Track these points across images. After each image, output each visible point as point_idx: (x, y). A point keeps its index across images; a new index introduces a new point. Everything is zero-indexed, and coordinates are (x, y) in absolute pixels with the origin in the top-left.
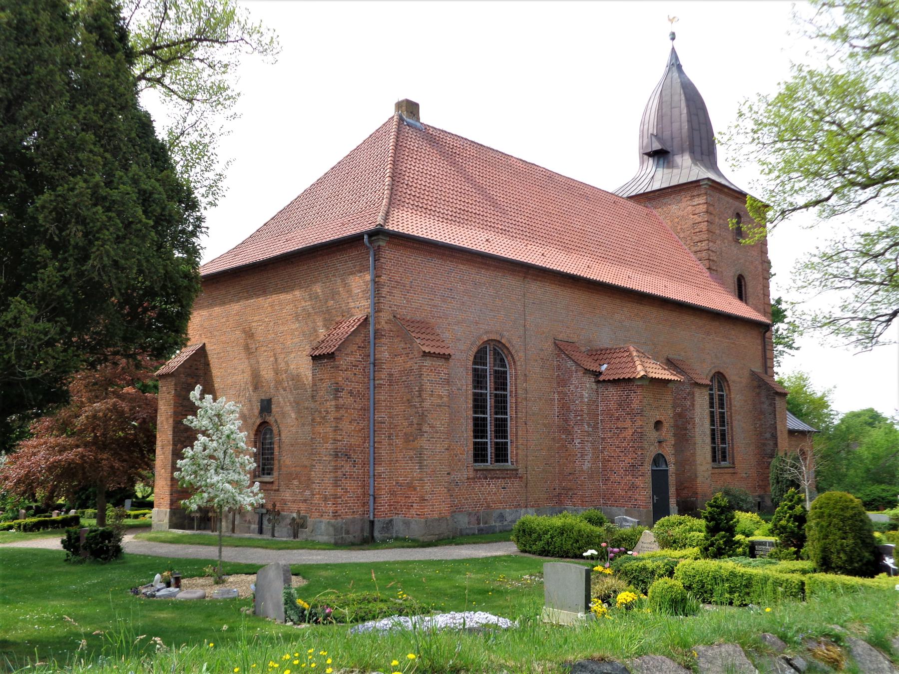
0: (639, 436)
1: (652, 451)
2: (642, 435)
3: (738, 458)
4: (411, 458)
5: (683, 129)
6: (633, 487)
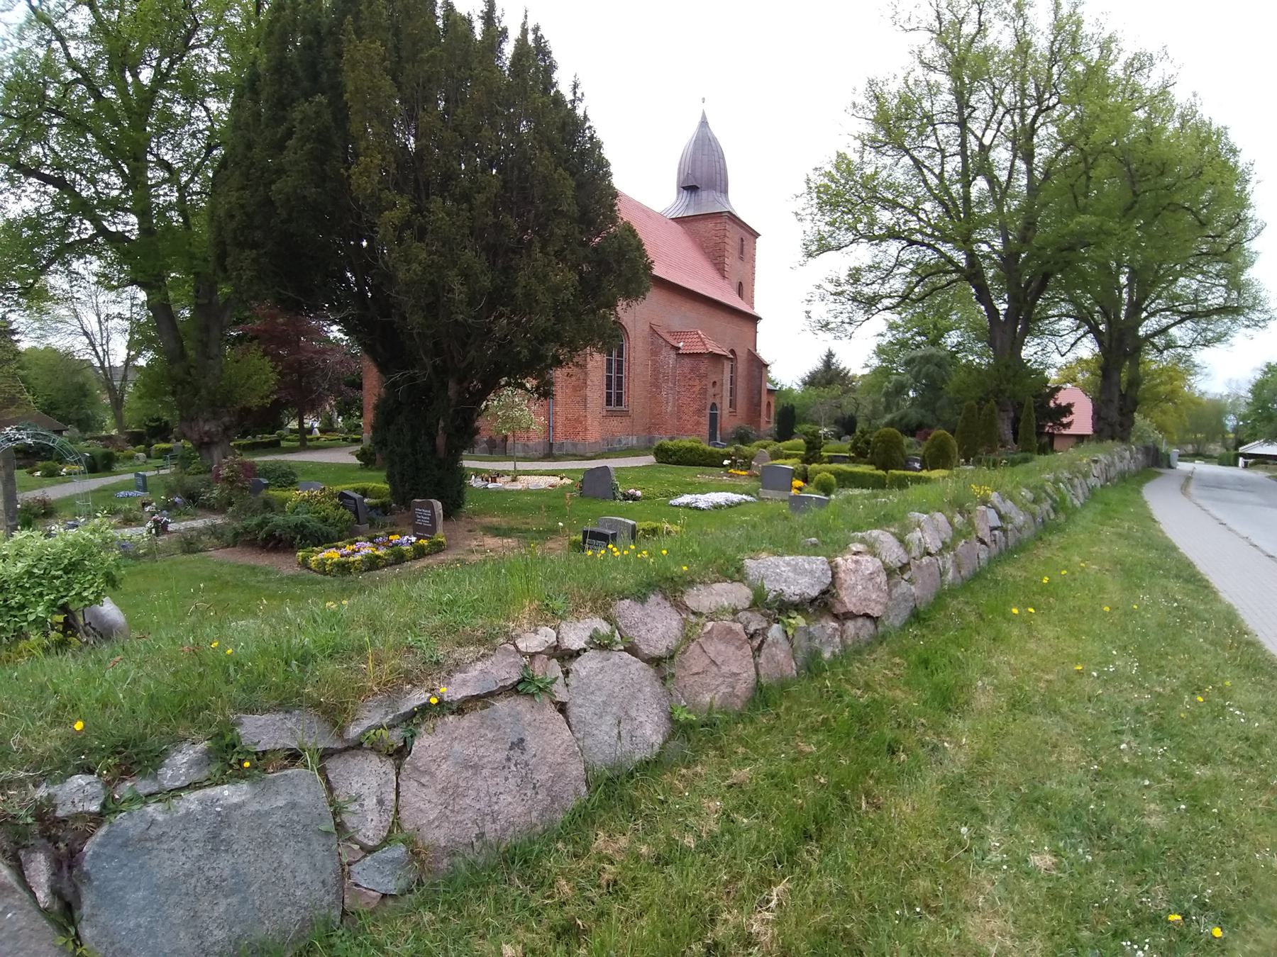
0: (704, 391)
1: (710, 401)
2: (706, 391)
6: (698, 423)
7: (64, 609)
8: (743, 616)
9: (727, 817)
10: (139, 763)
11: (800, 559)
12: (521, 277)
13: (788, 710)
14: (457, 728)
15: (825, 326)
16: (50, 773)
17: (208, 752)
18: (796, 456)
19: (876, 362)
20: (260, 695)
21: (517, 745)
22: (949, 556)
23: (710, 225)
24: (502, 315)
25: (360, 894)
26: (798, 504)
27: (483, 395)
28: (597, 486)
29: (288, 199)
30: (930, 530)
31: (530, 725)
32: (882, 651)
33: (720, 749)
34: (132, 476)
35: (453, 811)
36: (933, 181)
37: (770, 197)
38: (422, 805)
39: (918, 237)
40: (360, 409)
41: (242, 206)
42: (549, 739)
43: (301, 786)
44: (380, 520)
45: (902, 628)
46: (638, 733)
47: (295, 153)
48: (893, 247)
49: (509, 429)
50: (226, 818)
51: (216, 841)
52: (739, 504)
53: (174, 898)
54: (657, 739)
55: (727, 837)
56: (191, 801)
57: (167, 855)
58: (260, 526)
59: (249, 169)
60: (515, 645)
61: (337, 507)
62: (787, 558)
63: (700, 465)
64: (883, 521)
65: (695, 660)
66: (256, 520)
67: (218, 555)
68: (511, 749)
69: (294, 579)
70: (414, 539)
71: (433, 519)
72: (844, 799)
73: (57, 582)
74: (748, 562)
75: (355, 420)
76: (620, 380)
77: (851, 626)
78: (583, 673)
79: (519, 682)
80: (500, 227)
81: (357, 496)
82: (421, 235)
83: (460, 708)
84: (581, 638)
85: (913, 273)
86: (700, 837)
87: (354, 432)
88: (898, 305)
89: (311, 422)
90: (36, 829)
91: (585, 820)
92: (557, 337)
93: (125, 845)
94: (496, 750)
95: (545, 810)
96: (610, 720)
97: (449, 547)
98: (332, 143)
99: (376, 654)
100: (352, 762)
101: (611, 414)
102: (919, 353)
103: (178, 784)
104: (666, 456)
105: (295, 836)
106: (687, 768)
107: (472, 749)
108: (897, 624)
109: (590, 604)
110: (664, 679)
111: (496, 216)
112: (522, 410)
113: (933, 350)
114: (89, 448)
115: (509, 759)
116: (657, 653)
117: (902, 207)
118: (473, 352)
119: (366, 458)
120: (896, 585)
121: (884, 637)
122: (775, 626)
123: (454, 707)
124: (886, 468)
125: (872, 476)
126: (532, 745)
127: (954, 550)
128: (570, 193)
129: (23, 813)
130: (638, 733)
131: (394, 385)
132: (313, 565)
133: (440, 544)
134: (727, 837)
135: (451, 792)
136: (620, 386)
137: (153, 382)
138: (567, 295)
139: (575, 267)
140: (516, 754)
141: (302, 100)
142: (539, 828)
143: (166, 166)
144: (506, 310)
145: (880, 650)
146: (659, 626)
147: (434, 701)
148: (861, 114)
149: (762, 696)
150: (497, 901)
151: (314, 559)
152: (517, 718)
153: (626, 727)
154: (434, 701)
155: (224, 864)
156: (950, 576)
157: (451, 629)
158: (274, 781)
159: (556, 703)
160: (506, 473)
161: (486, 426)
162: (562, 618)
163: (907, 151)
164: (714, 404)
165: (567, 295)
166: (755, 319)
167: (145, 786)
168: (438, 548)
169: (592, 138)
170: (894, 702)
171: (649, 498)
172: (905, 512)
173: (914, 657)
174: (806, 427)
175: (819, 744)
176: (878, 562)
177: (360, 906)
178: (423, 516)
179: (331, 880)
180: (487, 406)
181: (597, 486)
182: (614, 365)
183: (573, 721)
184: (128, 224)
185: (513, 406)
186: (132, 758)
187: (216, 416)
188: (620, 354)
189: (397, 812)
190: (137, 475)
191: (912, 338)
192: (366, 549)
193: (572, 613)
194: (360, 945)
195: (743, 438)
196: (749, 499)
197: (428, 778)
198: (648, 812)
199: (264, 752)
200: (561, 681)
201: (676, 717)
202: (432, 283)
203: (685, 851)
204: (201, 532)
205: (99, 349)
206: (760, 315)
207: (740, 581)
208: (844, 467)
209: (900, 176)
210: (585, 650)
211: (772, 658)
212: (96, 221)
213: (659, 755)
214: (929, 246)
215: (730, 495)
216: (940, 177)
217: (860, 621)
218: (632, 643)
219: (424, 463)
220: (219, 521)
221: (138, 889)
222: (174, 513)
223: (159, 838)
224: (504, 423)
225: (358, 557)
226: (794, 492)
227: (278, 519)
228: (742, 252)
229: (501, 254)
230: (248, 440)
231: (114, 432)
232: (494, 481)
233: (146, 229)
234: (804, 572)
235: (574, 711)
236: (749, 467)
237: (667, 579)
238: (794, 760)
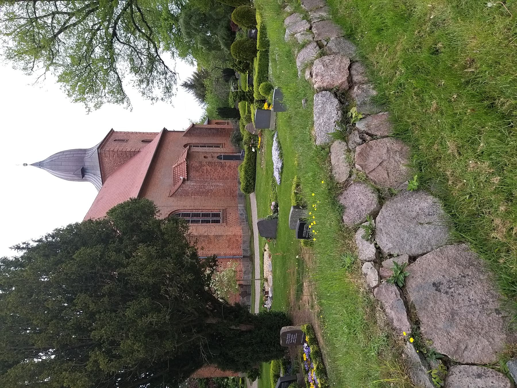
1: (216, 160)
3: (219, 142)
4: (218, 240)
6: (230, 167)
8: (351, 146)
9: (480, 156)
11: (315, 111)
12: (142, 279)
13: (409, 117)
15: (168, 89)
18: (249, 107)
19: (190, 57)
21: (437, 287)
22: (312, 15)
23: (106, 160)
26: (279, 107)
27: (215, 301)
28: (269, 229)
30: (296, 28)
31: (424, 279)
32: (372, 58)
33: (435, 159)
35: (482, 329)
36: (74, 20)
37: (87, 126)
39: (111, 30)
40: (223, 379)
42: (432, 267)
44: (294, 366)
45: (357, 45)
46: (427, 211)
48: (118, 46)
49: (236, 284)
52: (279, 142)
54: (430, 199)
55: (493, 157)
62: (315, 119)
64: (290, 58)
65: (380, 175)
68: (440, 291)
70: (306, 345)
71: (293, 332)
72: (468, 83)
74: (318, 143)
76: (204, 215)
77: (356, 78)
78: (390, 245)
79: (397, 285)
80: (111, 294)
82: (114, 344)
83: (416, 323)
85: (133, 33)
86: (493, 173)
87: (238, 382)
88: (154, 43)
91: (484, 245)
92: (180, 256)
94: (441, 300)
95: (478, 270)
96: (419, 229)
97: (310, 321)
99: (384, 377)
101: (225, 220)
102: (183, 30)
104: (250, 186)
106: (448, 180)
108: (354, 48)
109: (347, 241)
110: (392, 195)
111: (104, 296)
112: (223, 276)
113: (181, 20)
115: (447, 293)
116: (376, 200)
117: (92, 39)
118: (189, 309)
119: (255, 375)
120: (330, 50)
121: (363, 57)
122: (357, 126)
123: (415, 327)
124: (255, 51)
125: (260, 60)
126: (437, 278)
127: (307, 12)
130: (427, 211)
131: (209, 358)
133: (308, 328)
134: (493, 157)
135: (470, 329)
136: (207, 215)
138: (153, 250)
139: (135, 245)
140: (443, 288)
142: (491, 274)
145: (372, 59)
146: (359, 197)
147: (412, 340)
148: (31, 65)
149: (401, 134)
152: (420, 287)
153: (423, 219)
154: (412, 340)
156: (324, 14)
160: (262, 285)
162: (356, 258)
163: (55, 36)
164: (218, 157)
165: (153, 250)
166: (165, 131)
168: (311, 329)
169: (53, 236)
170: (405, 50)
171: (276, 197)
172: (285, 44)
173: (376, 38)
174: (231, 100)
175: (431, 98)
176: (316, 62)
178: (291, 339)
180: (222, 299)
181: (269, 229)
182: (195, 219)
183: (420, 252)
185: (221, 281)
188: (188, 215)
189: (485, 365)
191: (173, 34)
192: (313, 375)
193: (353, 252)
195: (238, 139)
196: (275, 136)
198: (477, 205)
200: (396, 260)
201: (416, 188)
202: (146, 336)
203: (502, 182)
206: (162, 129)
207: (330, 147)
208: (255, 77)
209: (72, 41)
210: (376, 244)
211: (378, 128)
213: (440, 198)
214: (116, 23)
215: (273, 148)
216: (71, 15)
217: (353, 72)
218: (370, 215)
225: (318, 381)
226: (271, 108)
228: (123, 140)
232: (267, 293)
234: (323, 108)
235: (415, 251)
236: (256, 136)
238: (442, 114)
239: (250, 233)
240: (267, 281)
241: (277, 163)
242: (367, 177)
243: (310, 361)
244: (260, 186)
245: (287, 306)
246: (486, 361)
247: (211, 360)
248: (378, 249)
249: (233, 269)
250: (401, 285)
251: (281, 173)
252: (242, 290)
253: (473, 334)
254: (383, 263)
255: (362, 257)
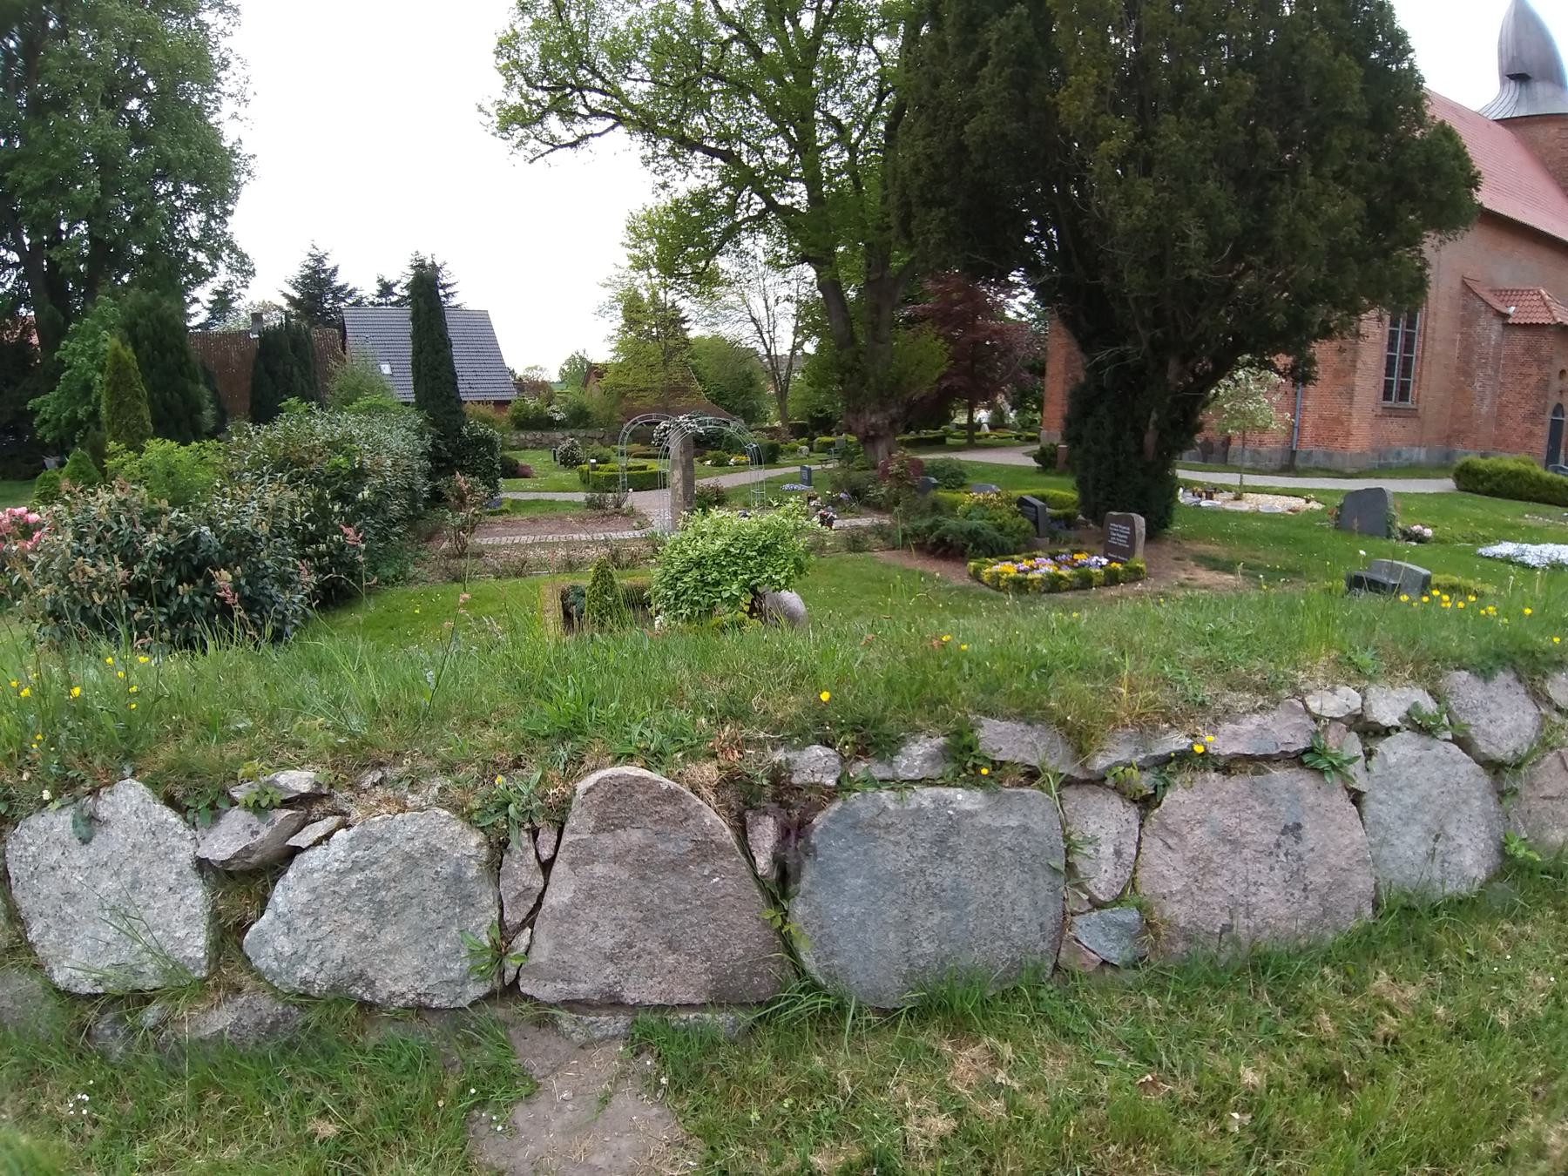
0: (1544, 384)
4: (1340, 394)
5: (355, 290)
6: (1531, 434)
7: (753, 590)
10: (877, 745)
14: (1220, 789)
16: (790, 738)
17: (944, 748)
20: (998, 700)
24: (1249, 267)
25: (1078, 951)
27: (1212, 379)
28: (1365, 515)
29: (985, 142)
31: (1312, 809)
34: (798, 469)
38: (1165, 872)
41: (930, 157)
42: (1335, 835)
43: (1031, 812)
44: (1064, 534)
46: (1454, 858)
47: (991, 83)
50: (957, 823)
51: (942, 846)
53: (891, 895)
56: (924, 797)
57: (892, 848)
58: (931, 529)
59: (936, 109)
60: (1303, 701)
61: (1015, 514)
63: (1529, 499)
66: (926, 522)
67: (884, 556)
68: (1283, 833)
69: (964, 591)
70: (1104, 561)
71: (1132, 540)
73: (751, 563)
75: (1030, 416)
76: (1407, 363)
78: (1392, 759)
79: (1306, 751)
80: (1253, 147)
81: (1038, 503)
82: (1146, 171)
83: (1228, 766)
84: (1394, 712)
89: (982, 415)
90: (768, 792)
93: (853, 827)
94: (1265, 829)
98: (1034, 62)
100: (1091, 799)
103: (911, 776)
104: (1472, 481)
105: (1023, 865)
107: (1234, 821)
109: (1410, 667)
110: (1502, 795)
112: (1259, 402)
114: (753, 440)
115: (1278, 846)
116: (1499, 755)
119: (1047, 460)
123: (1221, 763)
126: (1311, 834)
128: (1357, 86)
129: (760, 773)
130: (1454, 858)
131: (1098, 367)
132: (985, 578)
133: (1138, 571)
135: (1202, 867)
136: (1406, 371)
137: (820, 371)
138: (1351, 232)
140: (1288, 841)
141: (995, 16)
143: (836, 123)
144: (1257, 260)
146: (1507, 718)
150: (1237, 1012)
151: (987, 572)
152: (1297, 796)
155: (945, 874)
157: (1221, 667)
158: (1009, 796)
159: (1350, 791)
160: (1227, 488)
161: (1212, 422)
165: (1351, 232)
167: (879, 771)
168: (1135, 575)
171: (1442, 541)
177: (1075, 966)
178: (1118, 533)
179: (1049, 926)
180: (1217, 394)
181: (1365, 515)
183: (1368, 819)
184: (797, 195)
185: (1247, 395)
186: (871, 740)
187: (883, 406)
188: (1411, 324)
189: (1135, 871)
190: (803, 468)
192: (1046, 567)
194: (1071, 1008)
197: (1176, 840)
199: (1002, 763)
200: (1361, 762)
204: (868, 531)
205: (766, 336)
210: (1398, 729)
212: (765, 195)
219: (1125, 465)
220: (887, 522)
221: (858, 877)
222: (840, 508)
223: (887, 827)
224: (1233, 418)
227: (951, 523)
229: (1254, 182)
230: (911, 436)
231: (777, 424)
232: (1210, 497)
233: (815, 198)
235: (1371, 806)
237: (1526, 652)
239: (1349, 471)
240: (1236, 499)
241: (1535, 554)
242: (1552, 749)
243: (1072, 564)
244: (1473, 506)
245: (1182, 535)
246: (1142, 875)
247: (1095, 369)
248: (1387, 732)
249: (1273, 426)
250: (1306, 758)
251: (1507, 560)
252: (1217, 444)
253: (1193, 868)
254: (1354, 734)
255: (1373, 690)
